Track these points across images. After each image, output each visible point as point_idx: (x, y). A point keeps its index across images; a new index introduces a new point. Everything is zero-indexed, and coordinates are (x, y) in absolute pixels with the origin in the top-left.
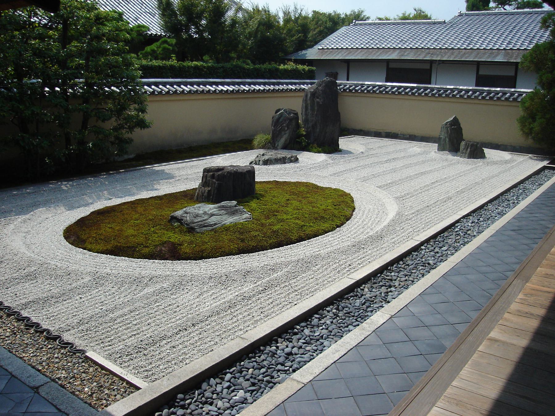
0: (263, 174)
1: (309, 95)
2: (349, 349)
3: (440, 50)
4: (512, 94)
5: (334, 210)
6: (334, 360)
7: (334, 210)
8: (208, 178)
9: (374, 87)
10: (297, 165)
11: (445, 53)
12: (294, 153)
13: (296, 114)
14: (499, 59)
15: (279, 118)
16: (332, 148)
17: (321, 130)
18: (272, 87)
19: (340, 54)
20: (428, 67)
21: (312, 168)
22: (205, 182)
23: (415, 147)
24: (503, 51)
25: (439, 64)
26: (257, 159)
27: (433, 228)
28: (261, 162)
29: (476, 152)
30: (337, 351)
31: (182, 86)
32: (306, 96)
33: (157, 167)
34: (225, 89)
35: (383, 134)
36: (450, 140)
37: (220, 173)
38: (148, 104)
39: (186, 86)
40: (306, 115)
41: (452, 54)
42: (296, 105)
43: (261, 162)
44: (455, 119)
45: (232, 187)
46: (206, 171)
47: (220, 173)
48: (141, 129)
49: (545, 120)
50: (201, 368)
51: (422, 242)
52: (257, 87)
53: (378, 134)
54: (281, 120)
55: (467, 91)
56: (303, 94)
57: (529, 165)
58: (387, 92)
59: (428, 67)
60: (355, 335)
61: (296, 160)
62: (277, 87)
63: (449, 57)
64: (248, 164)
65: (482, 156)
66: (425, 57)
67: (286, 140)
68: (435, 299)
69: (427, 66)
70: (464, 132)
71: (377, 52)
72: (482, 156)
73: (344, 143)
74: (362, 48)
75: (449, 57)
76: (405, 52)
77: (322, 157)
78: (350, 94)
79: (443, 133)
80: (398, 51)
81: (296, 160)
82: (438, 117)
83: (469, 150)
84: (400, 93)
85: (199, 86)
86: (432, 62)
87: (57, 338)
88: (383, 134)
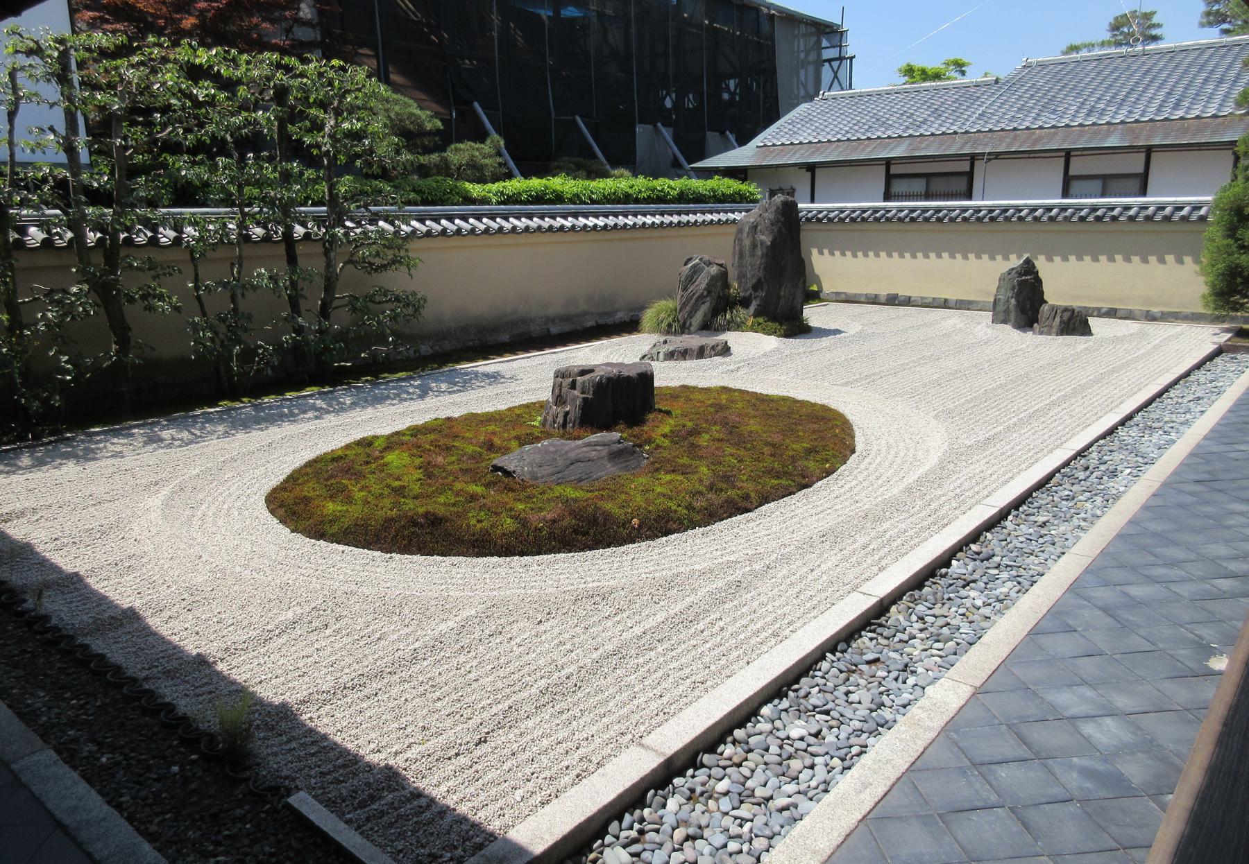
0: (667, 376)
2: (893, 779)
3: (990, 135)
4: (1144, 207)
5: (804, 446)
6: (864, 812)
7: (804, 446)
8: (564, 390)
9: (864, 212)
10: (727, 359)
11: (1002, 140)
16: (795, 327)
18: (675, 219)
19: (798, 155)
20: (967, 169)
21: (755, 362)
22: (560, 396)
23: (952, 320)
24: (1120, 126)
25: (989, 160)
26: (655, 351)
27: (1018, 479)
28: (661, 356)
29: (1075, 323)
30: (866, 786)
31: (511, 219)
32: (740, 231)
33: (465, 366)
34: (591, 224)
35: (883, 299)
36: (1018, 301)
39: (518, 218)
40: (741, 265)
41: (1015, 138)
43: (661, 356)
45: (621, 402)
46: (561, 374)
49: (657, 406)
50: (486, 566)
51: (1001, 510)
52: (649, 220)
55: (1049, 209)
57: (1206, 338)
58: (888, 220)
59: (967, 169)
60: (901, 740)
61: (725, 350)
62: (684, 218)
63: (1010, 144)
64: (637, 360)
65: (1085, 330)
66: (961, 149)
67: (705, 315)
68: (1063, 645)
69: (965, 167)
71: (868, 146)
72: (1085, 330)
74: (839, 140)
76: (921, 142)
77: (771, 342)
78: (819, 226)
80: (907, 142)
81: (725, 350)
84: (913, 220)
85: (542, 218)
86: (973, 158)
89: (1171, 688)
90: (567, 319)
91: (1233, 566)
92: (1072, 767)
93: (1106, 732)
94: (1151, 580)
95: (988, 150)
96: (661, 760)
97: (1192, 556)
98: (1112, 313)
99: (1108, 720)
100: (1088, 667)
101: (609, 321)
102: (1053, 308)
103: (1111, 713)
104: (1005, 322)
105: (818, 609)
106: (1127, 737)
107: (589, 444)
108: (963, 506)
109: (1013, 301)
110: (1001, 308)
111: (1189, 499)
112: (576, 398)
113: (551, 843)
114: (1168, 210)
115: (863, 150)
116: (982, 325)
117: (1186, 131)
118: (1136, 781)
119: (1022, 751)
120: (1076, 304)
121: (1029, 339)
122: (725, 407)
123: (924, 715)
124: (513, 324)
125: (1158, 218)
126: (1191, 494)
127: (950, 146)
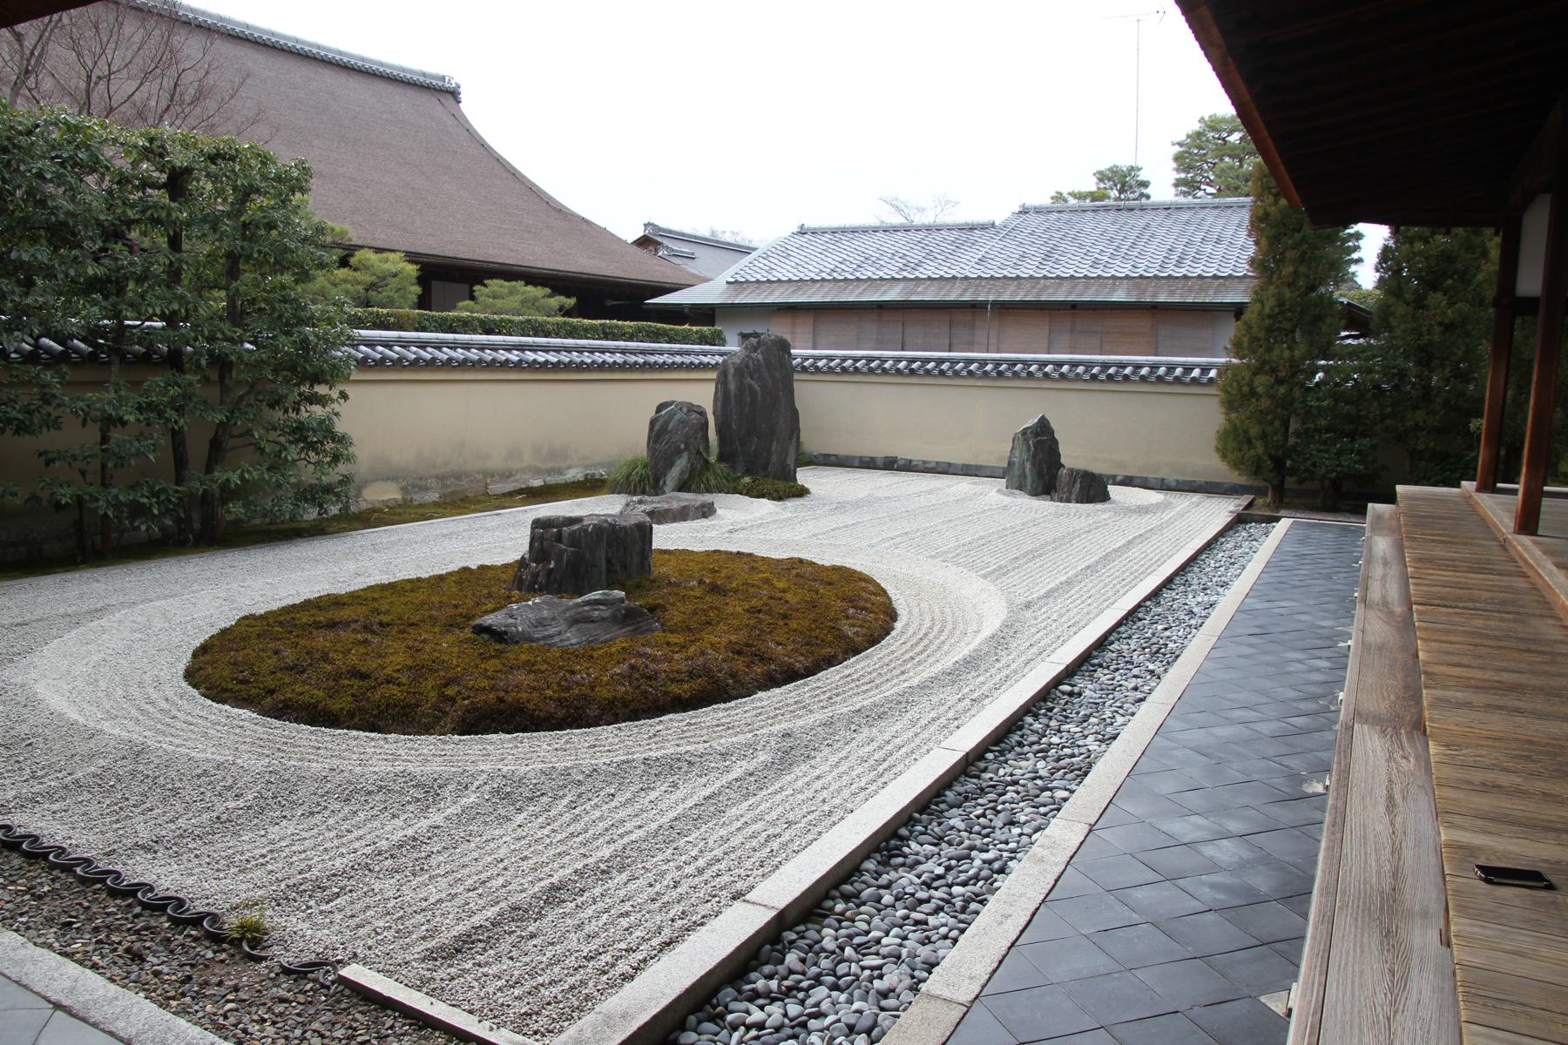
1: (732, 371)
5: (832, 619)
7: (832, 619)
12: (708, 498)
13: (702, 413)
14: (1119, 296)
15: (667, 423)
16: (785, 488)
17: (756, 444)
19: (777, 294)
23: (964, 485)
29: (1092, 489)
35: (880, 463)
36: (1033, 465)
37: (576, 527)
38: (349, 389)
41: (1018, 287)
42: (702, 395)
44: (1043, 418)
47: (576, 527)
48: (293, 183)
53: (869, 464)
54: (732, 386)
56: (714, 375)
57: (1216, 513)
63: (1015, 293)
65: (1104, 497)
67: (682, 472)
70: (1062, 449)
72: (1104, 497)
73: (804, 477)
75: (1015, 293)
77: (765, 506)
79: (1017, 453)
80: (902, 285)
82: (995, 420)
83: (1078, 485)
87: (203, 918)
88: (880, 463)
89: (1275, 810)
90: (506, 475)
91: (1303, 706)
92: (1203, 884)
93: (1225, 852)
94: (1230, 721)
95: (991, 298)
96: (773, 913)
97: (1264, 700)
98: (1128, 482)
99: (1225, 842)
100: (1193, 799)
101: (559, 479)
102: (1072, 470)
103: (1228, 836)
104: (1020, 488)
105: (1147, 573)
106: (1246, 854)
107: (588, 603)
108: (1077, 627)
109: (1028, 465)
110: (1016, 472)
111: (1249, 651)
112: (562, 552)
113: (674, 996)
114: (1179, 371)
115: (852, 292)
116: (991, 492)
117: (1190, 290)
118: (1264, 889)
119: (1152, 876)
120: (1097, 468)
121: (1044, 506)
122: (725, 574)
123: (1045, 853)
124: (441, 478)
125: (1170, 378)
126: (1250, 646)
127: (949, 292)
